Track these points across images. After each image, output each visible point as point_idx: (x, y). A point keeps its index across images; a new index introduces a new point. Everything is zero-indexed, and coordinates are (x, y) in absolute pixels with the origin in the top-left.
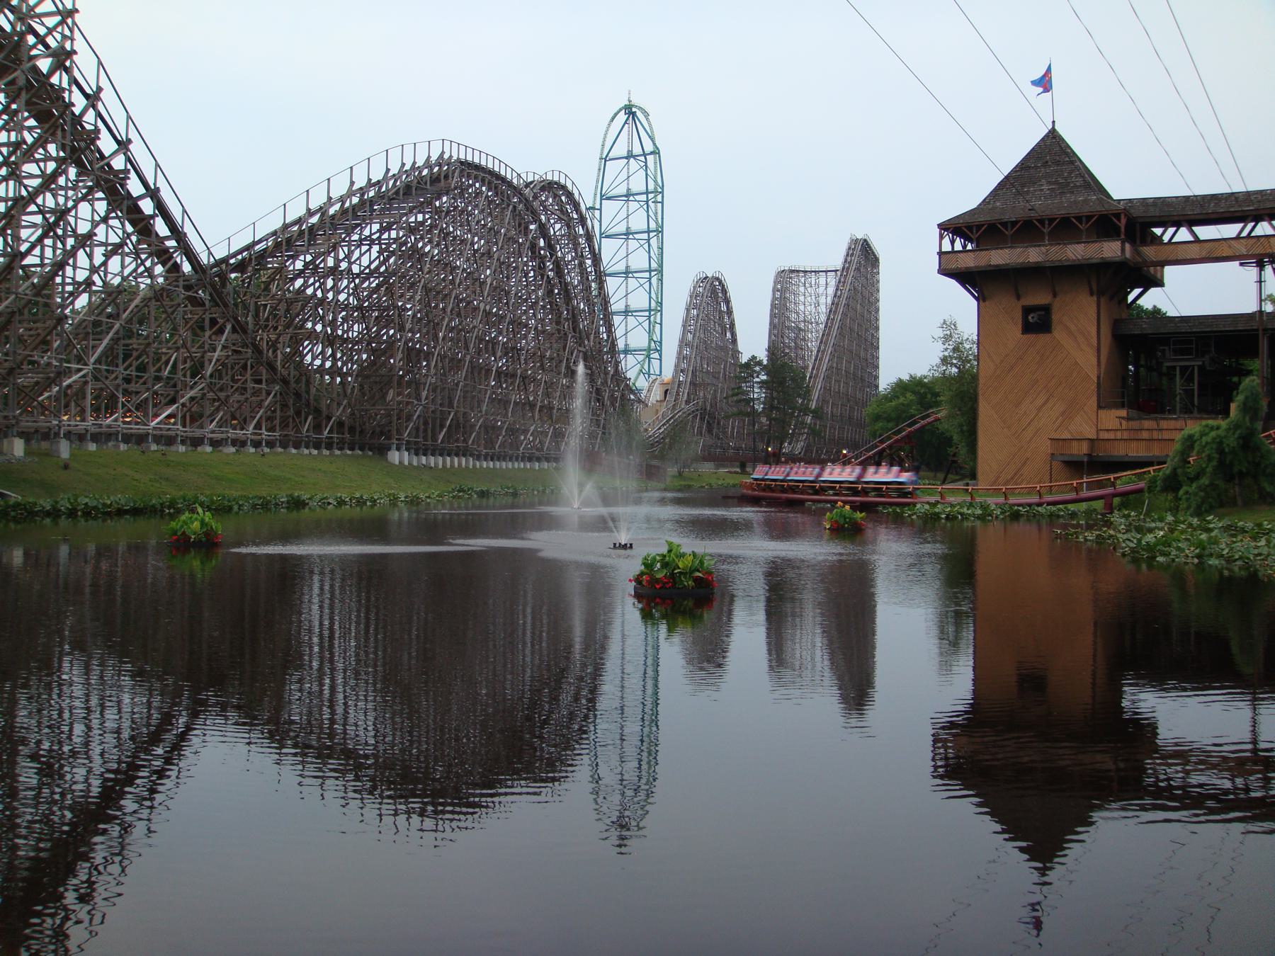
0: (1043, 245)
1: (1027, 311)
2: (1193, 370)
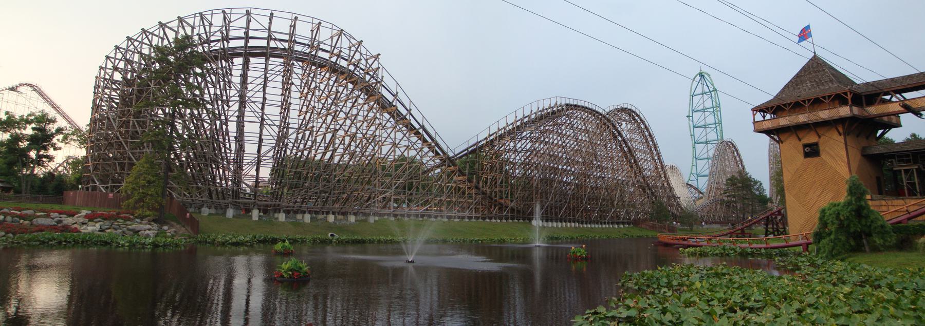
0: (806, 113)
1: (805, 146)
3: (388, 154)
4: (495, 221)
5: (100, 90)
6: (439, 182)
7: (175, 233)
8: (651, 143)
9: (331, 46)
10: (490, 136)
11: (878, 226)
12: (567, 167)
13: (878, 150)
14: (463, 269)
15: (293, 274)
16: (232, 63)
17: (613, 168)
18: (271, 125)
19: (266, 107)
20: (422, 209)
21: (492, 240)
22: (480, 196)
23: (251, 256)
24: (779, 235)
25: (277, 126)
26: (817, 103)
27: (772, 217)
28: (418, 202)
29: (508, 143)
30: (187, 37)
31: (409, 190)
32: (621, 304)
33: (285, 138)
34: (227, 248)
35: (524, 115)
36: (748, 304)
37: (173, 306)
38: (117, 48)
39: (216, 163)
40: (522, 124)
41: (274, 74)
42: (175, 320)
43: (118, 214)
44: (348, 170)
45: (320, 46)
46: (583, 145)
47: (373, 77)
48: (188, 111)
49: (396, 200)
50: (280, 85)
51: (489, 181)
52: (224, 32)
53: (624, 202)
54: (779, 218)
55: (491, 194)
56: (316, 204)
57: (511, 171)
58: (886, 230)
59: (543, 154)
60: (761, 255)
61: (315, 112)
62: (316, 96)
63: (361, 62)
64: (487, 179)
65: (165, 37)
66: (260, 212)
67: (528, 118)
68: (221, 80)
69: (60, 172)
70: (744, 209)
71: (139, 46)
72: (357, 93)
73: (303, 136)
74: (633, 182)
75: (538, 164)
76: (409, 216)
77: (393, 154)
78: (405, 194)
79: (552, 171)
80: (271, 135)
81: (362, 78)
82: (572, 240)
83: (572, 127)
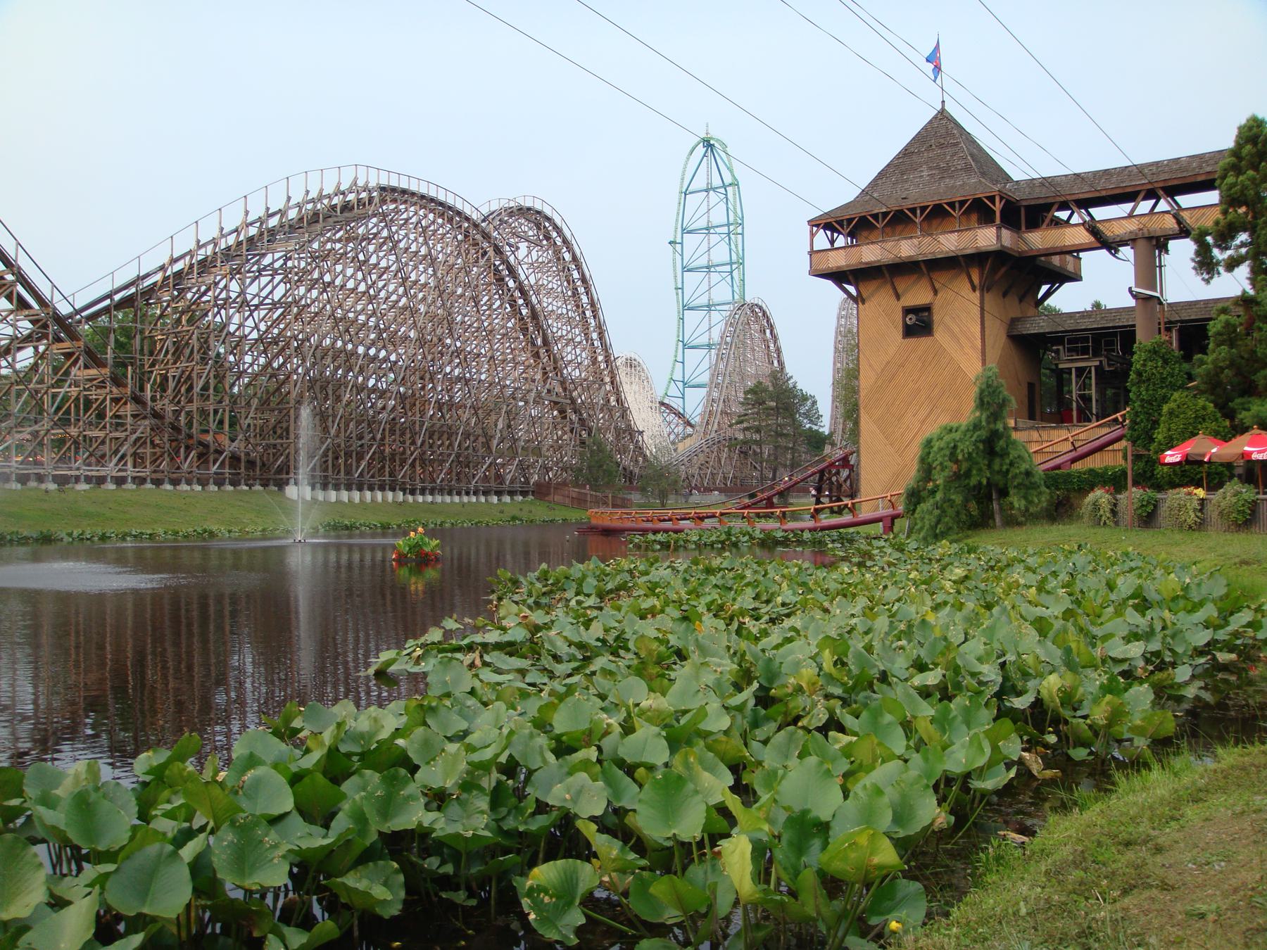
0: (915, 237)
1: (907, 311)
2: (1090, 372)
4: (188, 488)
8: (585, 299)
10: (174, 261)
11: (1020, 473)
12: (378, 351)
17: (492, 357)
22: (147, 422)
26: (937, 214)
35: (268, 209)
40: (261, 234)
46: (420, 295)
51: (171, 384)
53: (515, 440)
55: (177, 419)
59: (316, 314)
60: (800, 542)
64: (165, 378)
67: (278, 216)
74: (539, 394)
75: (303, 341)
83: (394, 247)
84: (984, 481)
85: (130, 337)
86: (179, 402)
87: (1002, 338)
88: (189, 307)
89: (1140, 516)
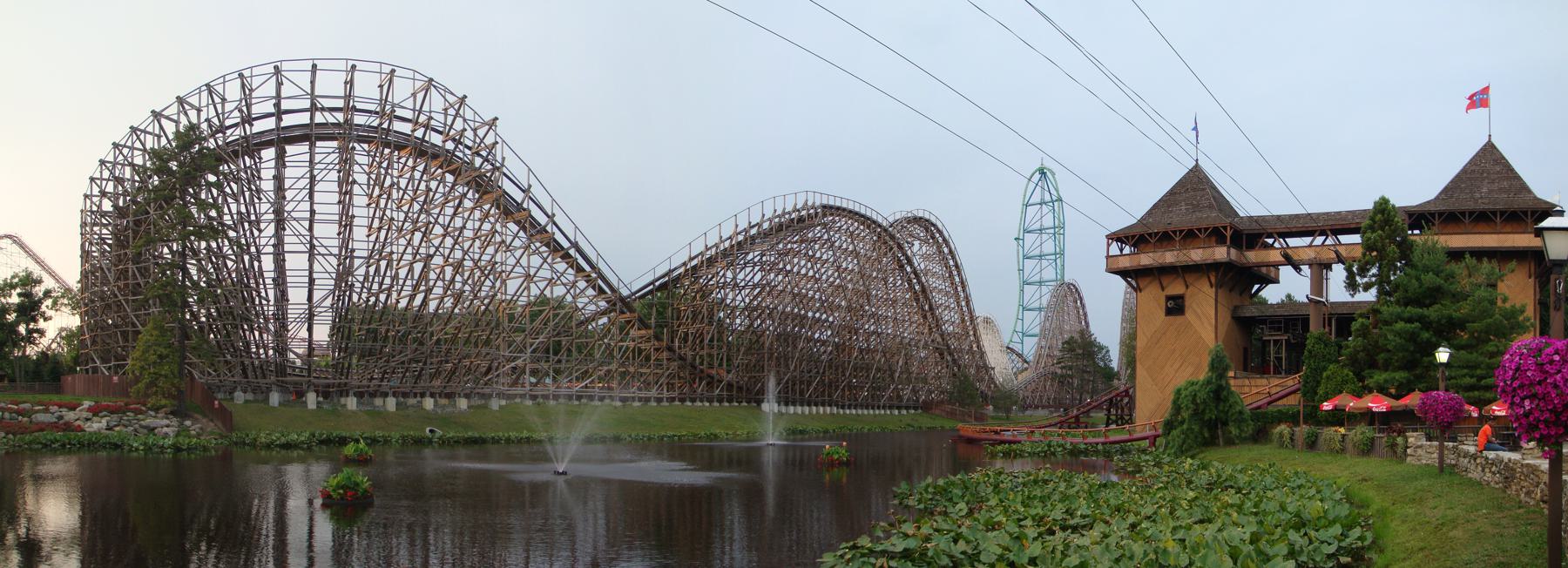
1: (1169, 298)
2: (1282, 344)
3: (518, 294)
5: (88, 228)
6: (606, 340)
7: (204, 433)
8: (957, 279)
9: (414, 110)
10: (691, 259)
11: (1236, 412)
12: (821, 315)
13: (1251, 311)
14: (649, 483)
15: (345, 492)
16: (260, 158)
17: (896, 318)
18: (326, 255)
19: (316, 226)
20: (578, 386)
21: (695, 435)
22: (676, 363)
23: (309, 465)
24: (1123, 424)
25: (335, 256)
26: (1190, 236)
27: (1116, 400)
28: (571, 374)
29: (722, 272)
30: (193, 127)
31: (556, 353)
32: (895, 531)
33: (348, 275)
34: (274, 452)
35: (750, 223)
36: (1072, 522)
37: (208, 537)
38: (102, 162)
39: (249, 323)
40: (746, 239)
41: (325, 169)
42: (212, 556)
43: (126, 404)
44: (453, 323)
45: (395, 111)
46: (849, 278)
47: (488, 161)
48: (203, 244)
49: (534, 372)
50: (335, 187)
51: (691, 338)
52: (245, 109)
53: (910, 373)
54: (1126, 400)
55: (695, 359)
56: (404, 380)
57: (728, 320)
58: (1244, 417)
59: (781, 291)
60: (1097, 452)
61: (394, 228)
62: (393, 201)
63: (466, 134)
65: (162, 134)
66: (317, 396)
68: (245, 189)
69: (54, 350)
70: (1082, 387)
71: (130, 155)
72: (460, 190)
73: (377, 270)
74: (926, 342)
76: (556, 397)
77: (525, 293)
78: (549, 361)
79: (796, 321)
80: (327, 272)
81: (468, 164)
82: (826, 435)
83: (832, 246)
84: (1214, 417)
85: (665, 308)
86: (695, 350)
87: (1229, 319)
88: (701, 288)
89: (1307, 443)
